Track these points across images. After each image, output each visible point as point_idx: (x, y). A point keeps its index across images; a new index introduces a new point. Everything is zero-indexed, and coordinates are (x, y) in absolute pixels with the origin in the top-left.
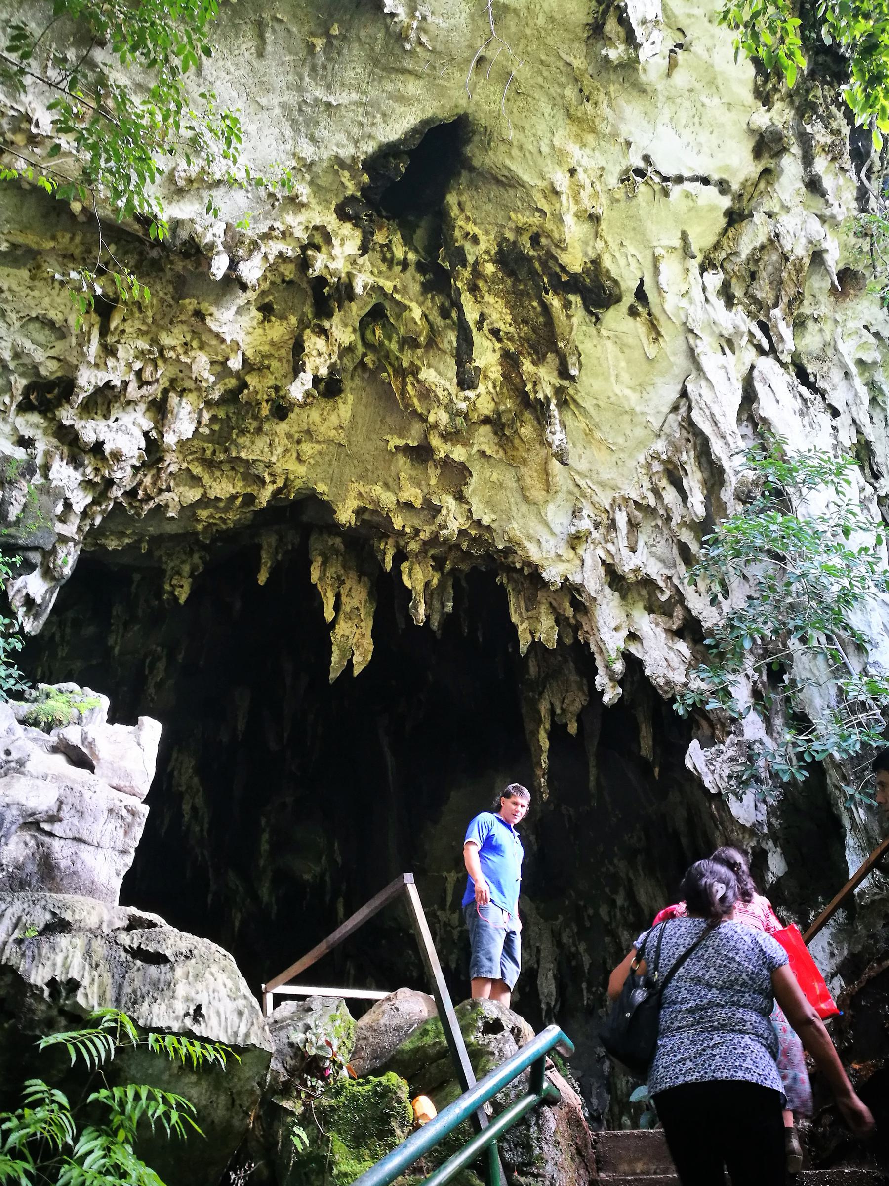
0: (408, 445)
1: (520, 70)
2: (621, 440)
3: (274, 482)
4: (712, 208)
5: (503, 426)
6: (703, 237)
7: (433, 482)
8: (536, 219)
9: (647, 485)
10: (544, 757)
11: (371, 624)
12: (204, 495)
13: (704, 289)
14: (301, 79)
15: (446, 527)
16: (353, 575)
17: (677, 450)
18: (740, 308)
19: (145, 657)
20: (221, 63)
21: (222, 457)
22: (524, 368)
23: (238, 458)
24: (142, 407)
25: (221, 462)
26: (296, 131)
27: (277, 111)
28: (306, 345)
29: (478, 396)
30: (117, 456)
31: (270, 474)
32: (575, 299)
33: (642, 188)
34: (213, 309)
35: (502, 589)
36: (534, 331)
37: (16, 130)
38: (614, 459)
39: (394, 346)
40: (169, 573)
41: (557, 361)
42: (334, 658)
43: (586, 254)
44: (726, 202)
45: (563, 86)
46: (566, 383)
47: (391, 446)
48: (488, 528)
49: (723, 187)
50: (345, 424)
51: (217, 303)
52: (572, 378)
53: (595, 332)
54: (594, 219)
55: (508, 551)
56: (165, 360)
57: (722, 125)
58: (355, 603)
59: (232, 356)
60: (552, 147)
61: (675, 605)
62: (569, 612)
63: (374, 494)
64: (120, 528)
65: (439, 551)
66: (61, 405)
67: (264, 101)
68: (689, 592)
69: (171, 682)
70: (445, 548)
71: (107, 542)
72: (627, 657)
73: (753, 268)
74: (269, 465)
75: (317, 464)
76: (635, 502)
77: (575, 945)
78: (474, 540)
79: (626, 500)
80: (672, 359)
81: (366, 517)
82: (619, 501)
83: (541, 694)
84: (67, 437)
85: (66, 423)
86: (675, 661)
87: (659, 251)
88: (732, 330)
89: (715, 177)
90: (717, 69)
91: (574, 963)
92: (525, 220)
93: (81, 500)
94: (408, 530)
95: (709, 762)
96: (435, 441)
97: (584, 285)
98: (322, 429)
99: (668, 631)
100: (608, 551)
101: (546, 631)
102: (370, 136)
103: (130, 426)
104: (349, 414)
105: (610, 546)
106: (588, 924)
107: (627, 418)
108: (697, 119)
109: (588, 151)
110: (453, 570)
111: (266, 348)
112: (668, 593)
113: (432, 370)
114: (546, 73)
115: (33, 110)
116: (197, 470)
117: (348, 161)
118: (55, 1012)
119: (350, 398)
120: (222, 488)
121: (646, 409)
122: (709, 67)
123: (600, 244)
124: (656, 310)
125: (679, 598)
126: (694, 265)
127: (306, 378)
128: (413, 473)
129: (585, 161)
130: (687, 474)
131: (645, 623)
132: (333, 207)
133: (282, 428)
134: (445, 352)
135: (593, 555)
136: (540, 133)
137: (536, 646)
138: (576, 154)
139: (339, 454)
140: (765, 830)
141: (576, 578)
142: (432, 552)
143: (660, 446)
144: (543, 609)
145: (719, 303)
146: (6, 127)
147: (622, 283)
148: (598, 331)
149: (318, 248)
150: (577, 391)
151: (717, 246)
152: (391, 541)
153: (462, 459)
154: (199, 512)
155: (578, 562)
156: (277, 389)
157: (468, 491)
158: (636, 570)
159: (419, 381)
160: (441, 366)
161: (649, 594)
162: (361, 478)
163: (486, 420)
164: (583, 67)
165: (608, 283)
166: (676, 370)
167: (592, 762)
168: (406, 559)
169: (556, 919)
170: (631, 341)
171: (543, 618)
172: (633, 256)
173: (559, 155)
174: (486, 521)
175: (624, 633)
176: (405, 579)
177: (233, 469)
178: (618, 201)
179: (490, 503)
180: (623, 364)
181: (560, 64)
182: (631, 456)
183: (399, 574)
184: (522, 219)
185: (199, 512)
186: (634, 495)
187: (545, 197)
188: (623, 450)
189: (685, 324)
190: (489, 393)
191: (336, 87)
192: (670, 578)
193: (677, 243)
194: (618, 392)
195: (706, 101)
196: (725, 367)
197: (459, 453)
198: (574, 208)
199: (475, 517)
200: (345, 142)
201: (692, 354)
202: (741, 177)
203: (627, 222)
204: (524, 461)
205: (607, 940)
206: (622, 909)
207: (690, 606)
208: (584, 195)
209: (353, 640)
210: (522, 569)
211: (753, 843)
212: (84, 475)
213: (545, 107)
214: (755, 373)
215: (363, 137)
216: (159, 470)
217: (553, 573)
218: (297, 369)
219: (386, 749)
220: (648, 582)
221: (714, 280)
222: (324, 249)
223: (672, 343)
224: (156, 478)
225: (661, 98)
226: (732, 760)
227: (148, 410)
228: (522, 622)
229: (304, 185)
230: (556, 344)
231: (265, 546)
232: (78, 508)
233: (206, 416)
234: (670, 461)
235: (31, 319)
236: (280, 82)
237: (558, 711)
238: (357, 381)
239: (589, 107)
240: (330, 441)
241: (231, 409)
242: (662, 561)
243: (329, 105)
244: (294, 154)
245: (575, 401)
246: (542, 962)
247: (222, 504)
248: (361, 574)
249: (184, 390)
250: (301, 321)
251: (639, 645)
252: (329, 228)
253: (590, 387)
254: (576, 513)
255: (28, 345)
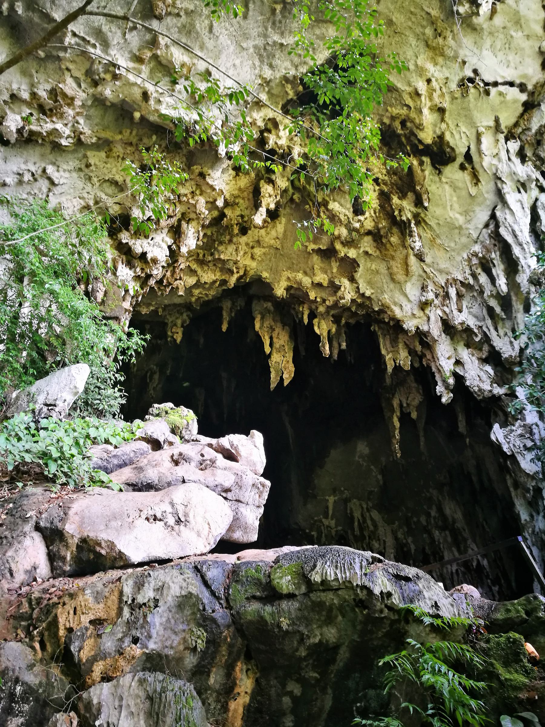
0: (320, 249)
1: (398, 18)
2: (453, 245)
3: (238, 272)
4: (515, 101)
5: (381, 237)
6: (507, 120)
7: (335, 270)
8: (404, 111)
9: (468, 271)
10: (397, 432)
11: (292, 355)
12: (198, 281)
13: (508, 151)
14: (266, 29)
15: (344, 298)
16: (279, 325)
17: (488, 251)
18: (530, 163)
19: (147, 372)
20: (223, 24)
21: (210, 258)
22: (394, 201)
23: (219, 259)
24: (166, 230)
25: (209, 261)
26: (262, 61)
27: (251, 50)
28: (262, 190)
29: (366, 219)
30: (155, 261)
31: (237, 268)
32: (426, 160)
33: (472, 91)
34: (210, 171)
35: (374, 333)
36: (400, 179)
37: (106, 71)
38: (448, 256)
39: (312, 189)
40: (170, 325)
41: (414, 197)
42: (273, 375)
43: (435, 132)
44: (524, 97)
45: (424, 27)
46: (420, 210)
47: (310, 249)
48: (369, 298)
49: (522, 87)
50: (280, 236)
51: (212, 167)
52: (426, 208)
53: (438, 179)
54: (441, 111)
55: (382, 311)
56: (180, 202)
57: (523, 49)
58: (282, 342)
59: (218, 198)
60: (416, 65)
61: (483, 344)
62: (419, 348)
63: (298, 278)
64: (149, 301)
65: (338, 313)
66: (121, 231)
67: (244, 45)
68: (493, 334)
69: (160, 386)
70: (341, 310)
71: (141, 309)
72: (455, 375)
73: (539, 138)
74: (236, 263)
75: (263, 260)
76: (461, 282)
77: (405, 538)
78: (360, 306)
79: (455, 280)
80: (486, 195)
81: (292, 292)
82: (450, 281)
83: (393, 395)
84: (125, 251)
85: (124, 241)
86: (484, 377)
87: (481, 129)
88: (525, 178)
89: (518, 82)
90: (522, 13)
91: (405, 549)
92: (397, 111)
93: (133, 287)
94: (318, 300)
95: (506, 437)
96: (338, 246)
97: (433, 151)
98: (267, 240)
99: (480, 359)
100: (444, 312)
101: (404, 359)
102: (305, 63)
103: (161, 242)
104: (282, 230)
105: (446, 309)
106: (414, 527)
107: (457, 231)
108: (507, 46)
109: (438, 67)
110: (347, 323)
111: (236, 192)
112: (480, 336)
113: (336, 203)
114: (413, 19)
115: (117, 59)
116: (194, 266)
117: (291, 79)
118: (383, 606)
119: (283, 220)
120: (208, 276)
121: (469, 226)
122: (517, 13)
123: (444, 126)
124: (477, 166)
125: (487, 339)
126: (501, 137)
127: (263, 210)
128: (322, 265)
129: (436, 75)
130: (494, 266)
131: (465, 354)
132: (280, 106)
133: (244, 239)
134: (345, 192)
135: (435, 314)
136: (409, 57)
137: (398, 369)
138: (431, 69)
139: (276, 254)
140: (541, 476)
141: (425, 328)
142: (332, 312)
143: (477, 248)
144: (401, 346)
145: (517, 161)
146: (101, 70)
147: (457, 150)
148: (440, 179)
149: (269, 131)
150: (426, 215)
151: (516, 125)
152: (306, 306)
153: (354, 257)
154: (194, 291)
155: (426, 318)
156: (242, 216)
157: (357, 276)
158: (462, 324)
159: (328, 210)
160: (342, 201)
161: (467, 336)
162: (289, 268)
163: (369, 233)
164: (437, 15)
165: (448, 150)
166: (488, 203)
167: (421, 434)
168: (315, 317)
169: (394, 523)
170: (460, 185)
171: (401, 351)
172: (464, 133)
173: (420, 71)
174: (368, 293)
175: (453, 360)
176: (316, 328)
177: (215, 265)
178: (456, 98)
179: (370, 283)
180: (455, 199)
181: (423, 14)
182: (459, 254)
183: (313, 325)
184: (395, 111)
185: (194, 291)
186: (460, 278)
187: (411, 97)
188: (454, 250)
189: (495, 174)
190: (371, 216)
191: (287, 33)
192: (481, 327)
193: (492, 123)
194: (451, 215)
195: (514, 34)
196: (520, 201)
197: (352, 253)
198: (429, 104)
199: (361, 292)
200: (290, 67)
201: (500, 194)
202: (534, 81)
203: (461, 112)
204: (393, 258)
205: (425, 536)
206: (435, 518)
207: (495, 344)
208: (435, 95)
209: (282, 365)
210: (389, 322)
211: (534, 484)
212: (135, 272)
213: (413, 41)
214: (539, 204)
215: (300, 64)
216: (174, 267)
217: (410, 325)
218: (257, 206)
219: (287, 424)
220: (468, 330)
221: (514, 146)
222: (273, 132)
223: (487, 187)
224: (173, 272)
225: (486, 33)
226: (521, 436)
227: (169, 231)
228: (388, 354)
229: (265, 94)
230: (414, 188)
231: (225, 308)
232: (132, 292)
233: (201, 234)
234: (484, 257)
235: (105, 181)
236: (254, 33)
237: (405, 405)
238: (288, 210)
239: (440, 40)
240: (270, 247)
241: (215, 229)
242: (476, 317)
243: (282, 45)
244: (260, 76)
245: (424, 221)
246: (387, 549)
247: (207, 286)
248: (284, 324)
249: (190, 219)
250: (257, 175)
251: (461, 368)
252: (278, 120)
253: (435, 212)
254: (424, 288)
255: (104, 196)
